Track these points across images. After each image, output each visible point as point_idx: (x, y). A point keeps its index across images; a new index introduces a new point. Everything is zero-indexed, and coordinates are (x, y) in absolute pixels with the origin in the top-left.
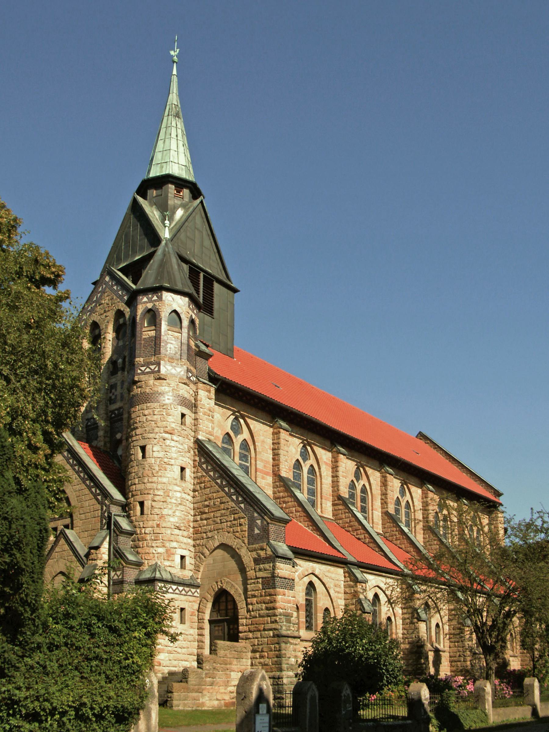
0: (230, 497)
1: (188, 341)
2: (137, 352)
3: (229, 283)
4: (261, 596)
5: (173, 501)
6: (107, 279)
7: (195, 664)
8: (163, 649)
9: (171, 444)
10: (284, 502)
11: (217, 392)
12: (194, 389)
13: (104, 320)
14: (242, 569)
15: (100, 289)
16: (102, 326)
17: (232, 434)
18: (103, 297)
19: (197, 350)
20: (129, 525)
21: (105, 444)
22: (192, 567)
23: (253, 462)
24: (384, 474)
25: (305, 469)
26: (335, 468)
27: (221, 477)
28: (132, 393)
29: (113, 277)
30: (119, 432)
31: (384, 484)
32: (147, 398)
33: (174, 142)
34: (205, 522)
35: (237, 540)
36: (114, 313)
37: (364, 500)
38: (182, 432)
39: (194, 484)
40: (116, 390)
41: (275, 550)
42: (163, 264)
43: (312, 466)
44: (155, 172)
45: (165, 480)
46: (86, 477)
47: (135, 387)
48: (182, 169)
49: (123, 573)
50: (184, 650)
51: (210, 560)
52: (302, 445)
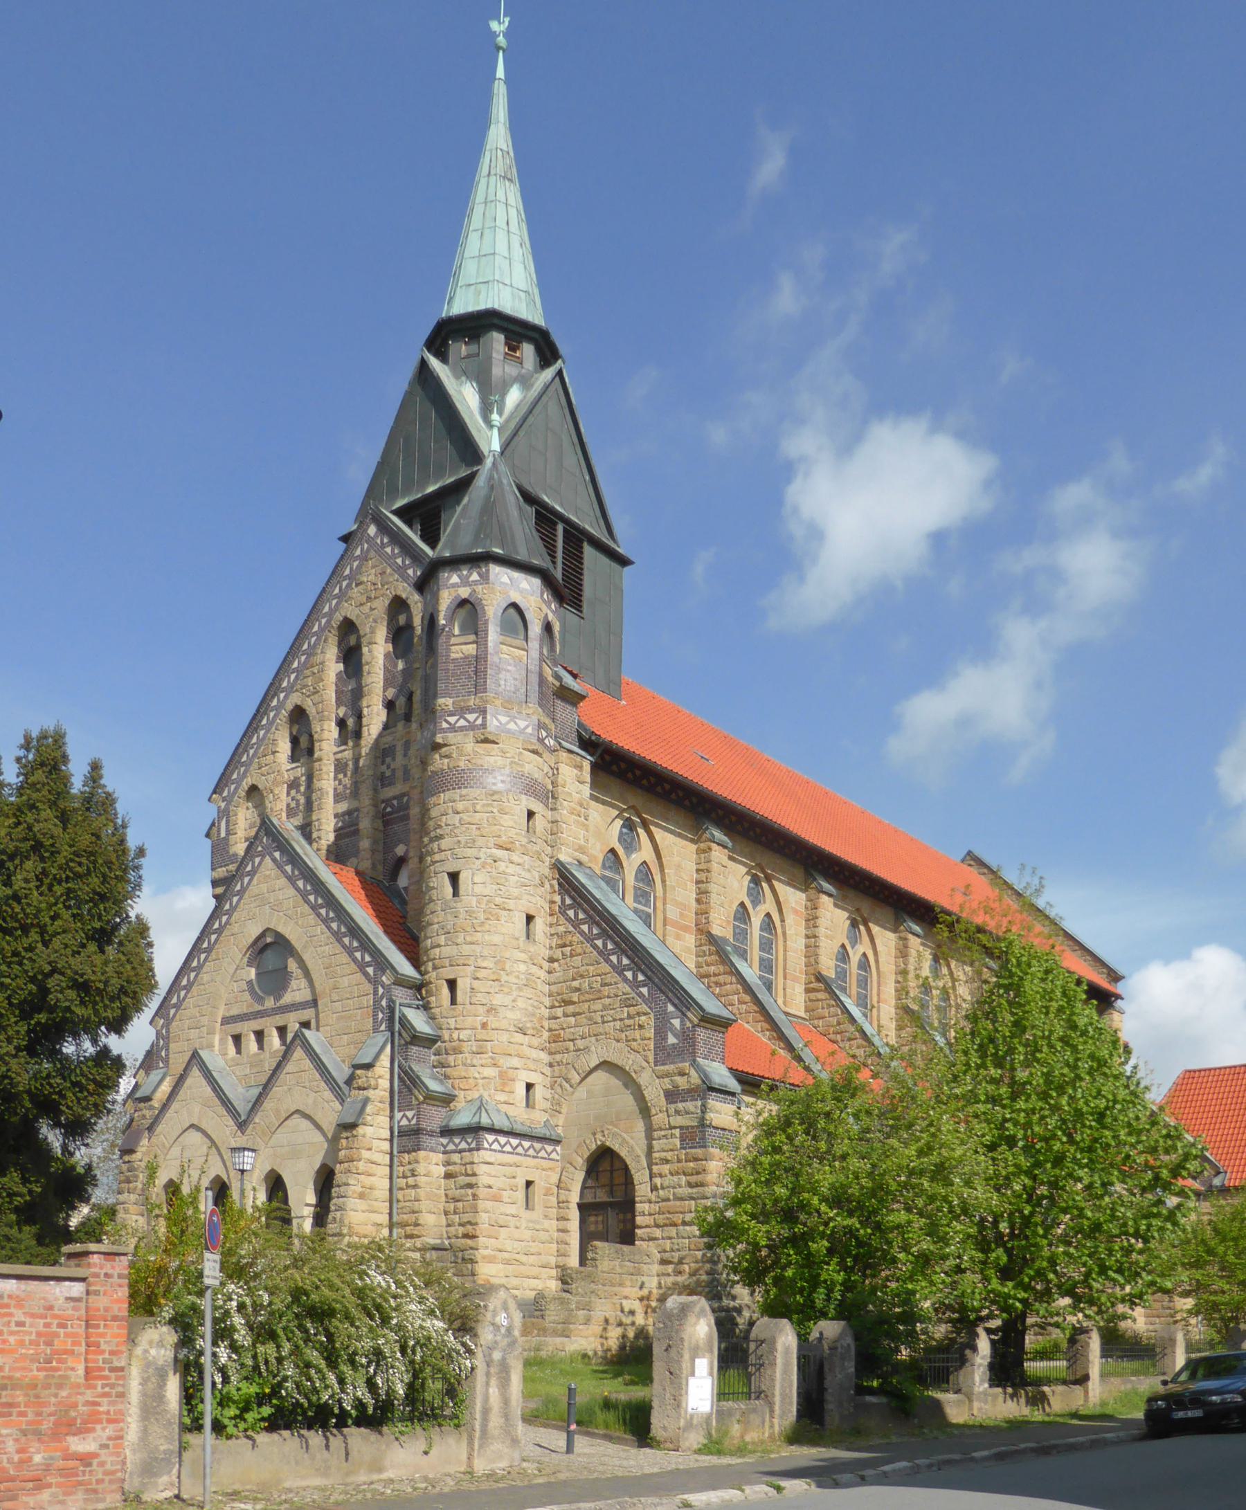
1: (541, 667)
2: (441, 686)
4: (679, 1161)
5: (512, 979)
6: (372, 530)
7: (554, 1285)
8: (495, 1257)
9: (508, 870)
10: (717, 984)
11: (595, 767)
13: (367, 617)
15: (358, 552)
16: (364, 629)
17: (621, 851)
18: (364, 569)
20: (428, 1023)
21: (374, 866)
22: (547, 1105)
23: (659, 905)
24: (903, 935)
25: (757, 920)
26: (812, 920)
27: (604, 934)
28: (431, 768)
29: (384, 527)
30: (400, 842)
32: (457, 779)
34: (572, 1019)
35: (633, 1056)
36: (387, 602)
37: (864, 983)
38: (529, 846)
39: (551, 948)
40: (394, 759)
43: (768, 915)
44: (462, 304)
45: (496, 939)
46: (343, 929)
47: (437, 756)
49: (418, 1115)
50: (532, 1259)
51: (581, 1092)
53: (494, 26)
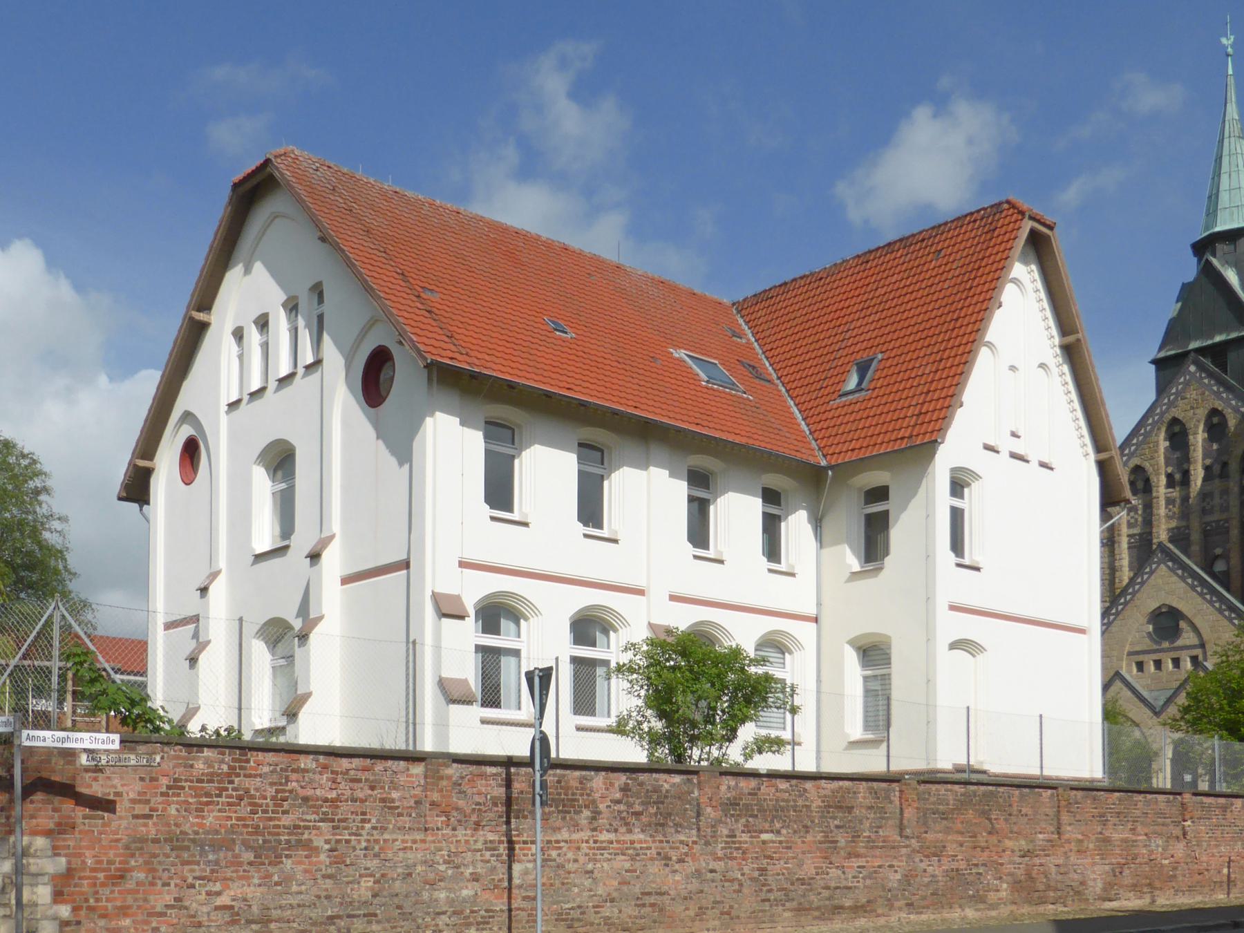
16: (1190, 425)
53: (1224, 41)
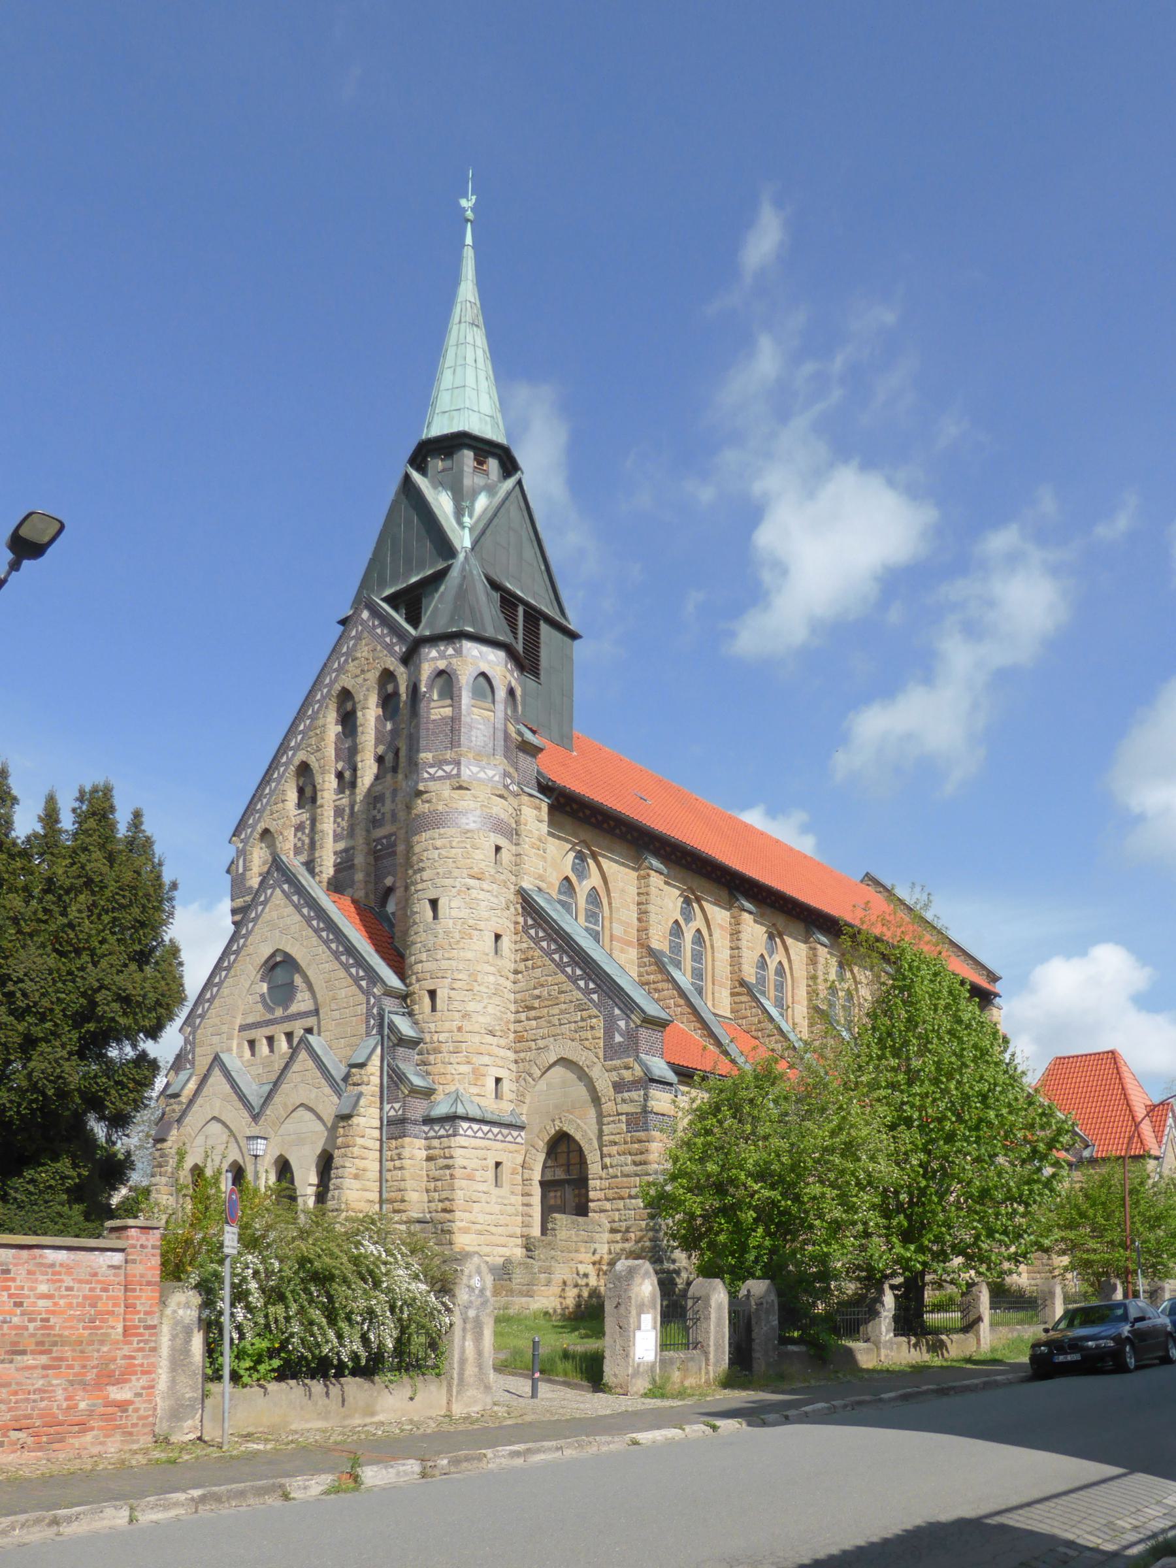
0: (575, 982)
1: (505, 725)
2: (423, 743)
3: (565, 623)
4: (626, 1143)
6: (365, 615)
8: (469, 1228)
10: (656, 990)
11: (552, 809)
12: (515, 804)
14: (596, 1100)
15: (354, 633)
16: (359, 697)
17: (574, 879)
19: (520, 739)
20: (412, 1027)
21: (367, 895)
22: (513, 1096)
23: (607, 923)
25: (689, 935)
26: (735, 934)
27: (560, 949)
29: (375, 612)
30: (389, 874)
31: (813, 960)
32: (436, 821)
33: (470, 372)
34: (534, 1022)
36: (378, 674)
37: (780, 987)
38: (497, 876)
41: (647, 1069)
42: (462, 593)
43: (698, 931)
44: (438, 428)
47: (419, 801)
48: (486, 423)
49: (404, 1106)
50: (500, 1230)
51: (542, 1085)
52: (572, 855)
53: (464, 203)
